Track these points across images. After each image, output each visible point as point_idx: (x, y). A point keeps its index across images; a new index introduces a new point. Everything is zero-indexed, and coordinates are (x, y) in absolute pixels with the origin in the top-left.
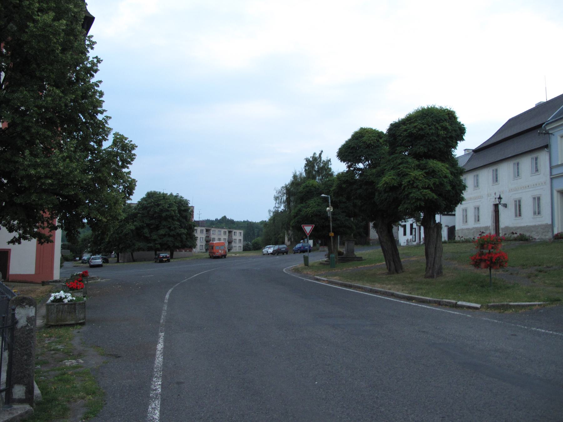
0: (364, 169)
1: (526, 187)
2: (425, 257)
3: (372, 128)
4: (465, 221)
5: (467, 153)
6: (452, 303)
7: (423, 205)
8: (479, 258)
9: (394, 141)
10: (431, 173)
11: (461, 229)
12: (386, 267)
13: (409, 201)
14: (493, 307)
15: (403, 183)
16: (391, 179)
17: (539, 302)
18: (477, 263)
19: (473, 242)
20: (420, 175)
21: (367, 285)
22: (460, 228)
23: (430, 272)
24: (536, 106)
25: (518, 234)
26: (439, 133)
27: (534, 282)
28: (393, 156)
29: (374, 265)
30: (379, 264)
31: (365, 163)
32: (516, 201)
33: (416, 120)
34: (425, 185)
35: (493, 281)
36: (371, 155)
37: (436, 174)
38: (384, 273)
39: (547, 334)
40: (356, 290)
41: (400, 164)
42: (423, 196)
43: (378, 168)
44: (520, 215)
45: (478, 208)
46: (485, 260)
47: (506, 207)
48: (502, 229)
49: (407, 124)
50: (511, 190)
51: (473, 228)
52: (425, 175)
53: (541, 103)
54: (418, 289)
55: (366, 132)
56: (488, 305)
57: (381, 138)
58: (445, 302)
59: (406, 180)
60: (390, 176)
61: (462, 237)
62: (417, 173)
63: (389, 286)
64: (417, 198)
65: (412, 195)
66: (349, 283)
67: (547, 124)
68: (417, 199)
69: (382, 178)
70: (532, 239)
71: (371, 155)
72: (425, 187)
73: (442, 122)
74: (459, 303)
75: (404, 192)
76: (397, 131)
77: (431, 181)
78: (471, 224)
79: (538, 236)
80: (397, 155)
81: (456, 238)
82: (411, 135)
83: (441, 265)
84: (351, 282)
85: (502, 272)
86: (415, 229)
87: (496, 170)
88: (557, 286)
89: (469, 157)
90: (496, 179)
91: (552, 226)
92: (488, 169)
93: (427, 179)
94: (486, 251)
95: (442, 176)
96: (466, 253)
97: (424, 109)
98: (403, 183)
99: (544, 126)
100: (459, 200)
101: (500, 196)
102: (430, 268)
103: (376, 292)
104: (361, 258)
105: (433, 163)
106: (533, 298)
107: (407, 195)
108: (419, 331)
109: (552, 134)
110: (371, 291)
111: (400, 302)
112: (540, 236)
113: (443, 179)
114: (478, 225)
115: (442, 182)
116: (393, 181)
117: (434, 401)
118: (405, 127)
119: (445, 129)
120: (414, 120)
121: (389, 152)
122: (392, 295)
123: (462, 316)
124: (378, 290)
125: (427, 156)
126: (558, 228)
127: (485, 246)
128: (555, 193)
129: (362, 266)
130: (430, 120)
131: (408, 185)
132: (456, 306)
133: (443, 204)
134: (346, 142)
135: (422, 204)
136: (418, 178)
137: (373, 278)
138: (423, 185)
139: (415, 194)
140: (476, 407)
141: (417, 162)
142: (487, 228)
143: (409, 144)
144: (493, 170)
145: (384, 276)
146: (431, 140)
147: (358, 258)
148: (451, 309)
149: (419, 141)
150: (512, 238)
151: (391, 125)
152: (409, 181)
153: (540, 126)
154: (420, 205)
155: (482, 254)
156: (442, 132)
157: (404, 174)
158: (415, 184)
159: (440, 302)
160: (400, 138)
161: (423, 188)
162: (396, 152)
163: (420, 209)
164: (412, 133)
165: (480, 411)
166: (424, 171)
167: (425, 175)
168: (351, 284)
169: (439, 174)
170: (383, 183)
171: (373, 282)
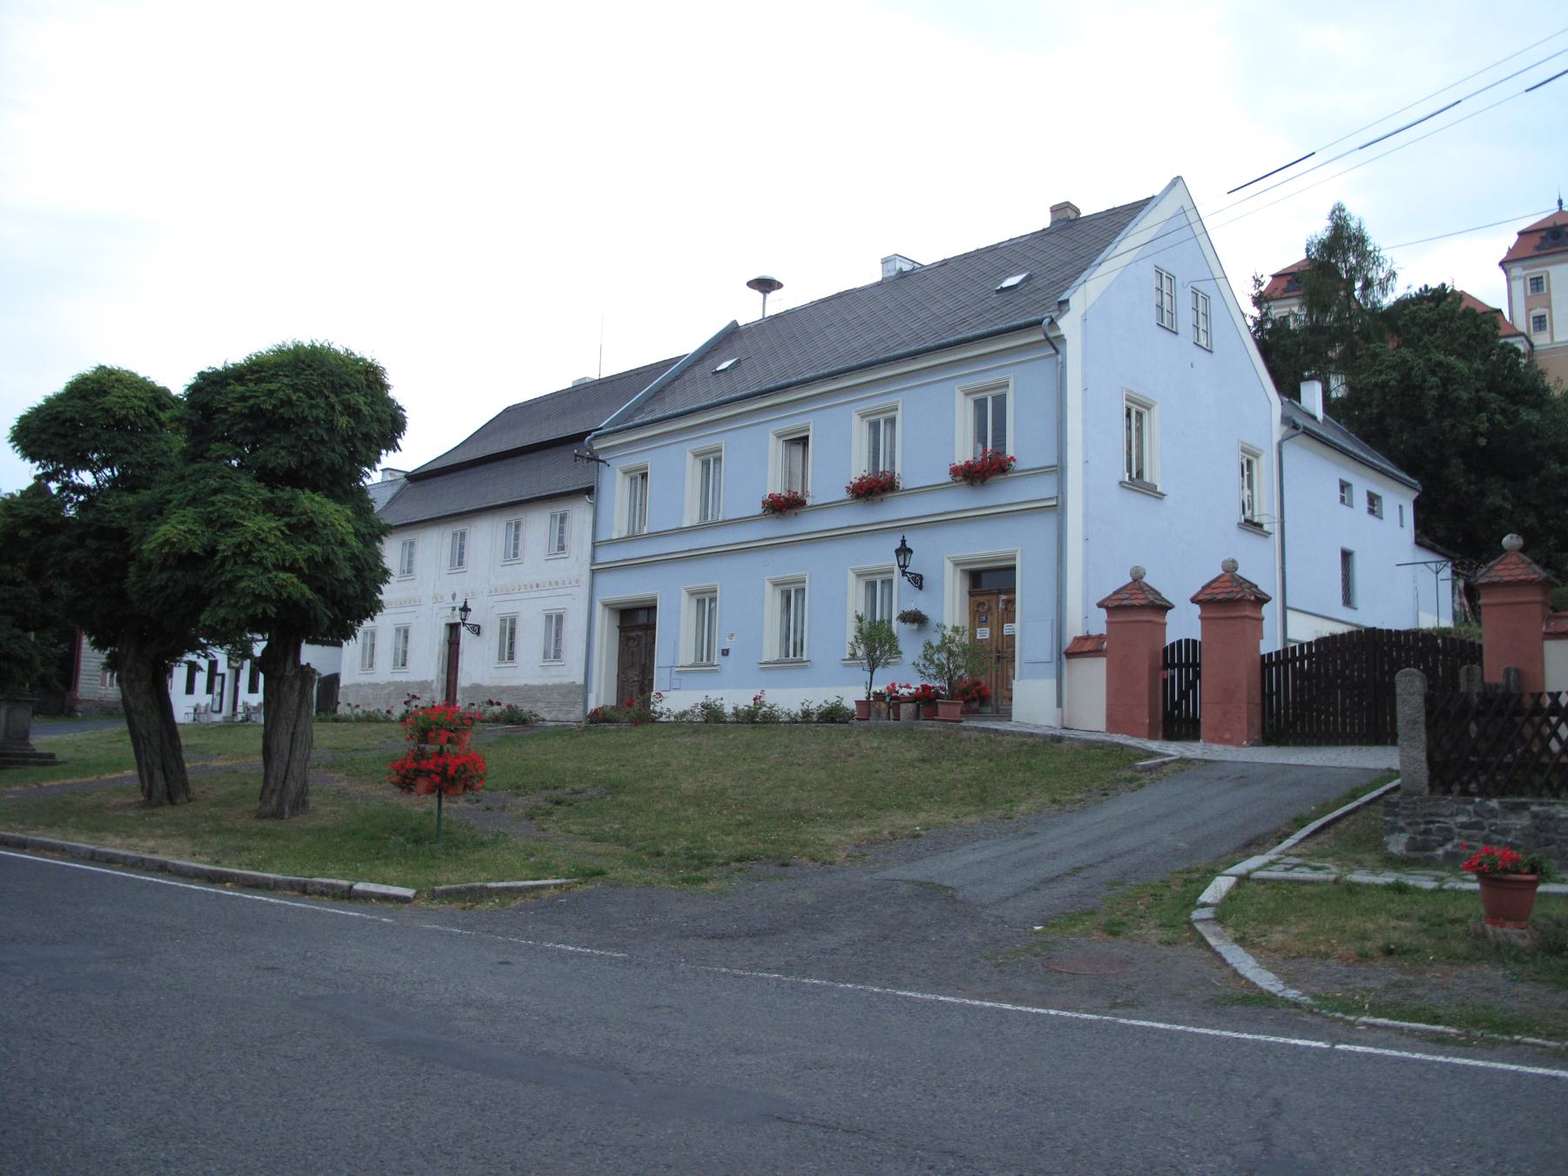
0: (95, 489)
1: (531, 587)
2: (259, 760)
3: (134, 371)
4: (369, 662)
5: (390, 478)
6: (341, 887)
7: (273, 616)
8: (415, 764)
9: (203, 423)
10: (304, 529)
11: (352, 685)
12: (137, 782)
13: (233, 601)
14: (448, 894)
15: (222, 547)
16: (185, 532)
17: (556, 878)
18: (406, 780)
19: (387, 720)
20: (271, 529)
21: (79, 841)
22: (352, 682)
23: (274, 801)
24: (574, 387)
25: (504, 707)
26: (335, 422)
27: (543, 830)
28: (196, 466)
29: (95, 777)
30: (114, 776)
31: (100, 470)
32: (503, 620)
33: (276, 375)
34: (284, 560)
35: (443, 828)
36: (125, 451)
37: (317, 532)
38: (129, 805)
39: (579, 955)
40: (43, 857)
41: (216, 492)
42: (276, 590)
43: (145, 495)
44: (511, 658)
45: (406, 632)
46: (429, 773)
47: (478, 634)
48: (464, 689)
49: (250, 380)
50: (496, 590)
51: (389, 683)
52: (287, 532)
53: (587, 381)
54: (240, 850)
55: (117, 380)
56: (434, 891)
57: (163, 407)
58: (321, 883)
59: (230, 541)
60: (183, 523)
61: (358, 706)
62: (264, 524)
63: (151, 843)
64: (260, 593)
65: (243, 584)
66: (17, 835)
67: (596, 437)
68: (259, 598)
69: (158, 525)
70: (536, 721)
71: (125, 451)
72: (284, 564)
73: (348, 393)
74: (359, 886)
75: (223, 573)
76: (217, 397)
77: (300, 549)
78: (384, 672)
79: (550, 712)
80: (208, 464)
81: (339, 708)
82: (255, 413)
83: (305, 784)
84: (21, 831)
85: (466, 804)
86: (223, 675)
87: (463, 535)
88: (596, 840)
89: (395, 489)
90: (459, 559)
91: (586, 688)
92: (442, 529)
93: (292, 542)
94: (431, 748)
95: (333, 541)
96: (368, 750)
97: (303, 346)
98: (222, 547)
99: (590, 441)
100: (368, 606)
101: (466, 603)
102: (273, 791)
103: (110, 860)
104: (52, 756)
105: (313, 500)
106: (543, 869)
107: (230, 584)
108: (259, 967)
109: (604, 461)
110: (93, 857)
111: (187, 889)
112: (554, 713)
113: (335, 548)
114: (401, 677)
115: (332, 557)
116: (191, 538)
117: (330, 1148)
118: (241, 389)
119: (353, 412)
120: (271, 372)
121: (184, 452)
122: (162, 868)
123: (370, 920)
124: (115, 855)
125: (294, 479)
126: (598, 696)
127: (432, 735)
128: (599, 608)
129: (56, 783)
130: (315, 378)
131: (234, 554)
132: (349, 895)
133: (324, 613)
134: (48, 400)
135: (269, 612)
136: (266, 537)
137: (96, 818)
138: (277, 560)
139: (253, 582)
140: (439, 1146)
141: (265, 493)
142: (425, 686)
143: (249, 438)
144: (455, 535)
145: (132, 814)
147: (41, 755)
148: (337, 903)
149: (277, 435)
150: (487, 715)
151: (202, 375)
152: (239, 545)
153: (579, 438)
154: (264, 612)
155: (422, 753)
156: (343, 422)
157: (224, 521)
158: (255, 555)
159: (305, 884)
160: (224, 417)
161: (277, 567)
162: (208, 455)
163: (258, 625)
164: (261, 410)
165: (448, 1154)
166: (286, 519)
167: (287, 532)
168: (24, 836)
169: (327, 534)
170: (160, 540)
171: (98, 830)
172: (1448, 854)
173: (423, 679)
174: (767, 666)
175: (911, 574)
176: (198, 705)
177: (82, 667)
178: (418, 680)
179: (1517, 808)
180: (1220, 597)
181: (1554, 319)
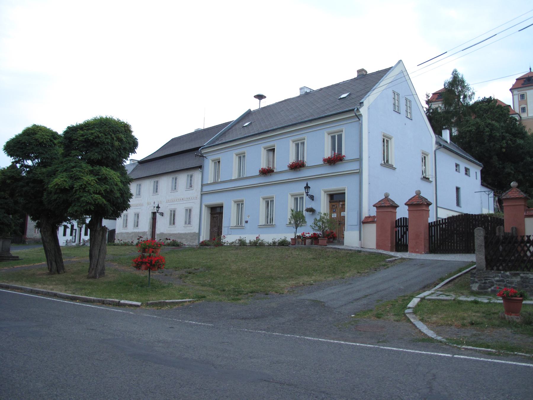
0: (32, 166)
1: (181, 200)
2: (88, 258)
3: (46, 126)
4: (126, 225)
5: (132, 163)
6: (116, 302)
7: (93, 209)
8: (141, 260)
9: (69, 144)
10: (103, 180)
11: (120, 233)
12: (47, 266)
13: (79, 204)
14: (152, 304)
15: (75, 186)
16: (63, 181)
17: (189, 299)
18: (138, 265)
19: (132, 245)
20: (92, 180)
21: (27, 286)
22: (120, 232)
23: (93, 272)
24: (195, 132)
25: (171, 240)
27: (185, 282)
28: (67, 159)
29: (32, 264)
30: (39, 264)
32: (171, 211)
33: (94, 128)
34: (96, 191)
35: (151, 282)
36: (42, 153)
37: (108, 181)
38: (44, 274)
39: (197, 325)
40: (15, 291)
41: (73, 167)
42: (94, 201)
43: (49, 169)
44: (174, 224)
45: (138, 215)
46: (146, 263)
47: (163, 216)
48: (158, 235)
49: (85, 129)
50: (169, 201)
51: (132, 232)
52: (97, 181)
53: (200, 129)
54: (81, 289)
55: (40, 129)
56: (147, 303)
57: (55, 138)
58: (109, 300)
59: (78, 184)
60: (62, 178)
61: (122, 240)
62: (90, 178)
63: (51, 287)
64: (88, 202)
65: (83, 199)
66: (6, 284)
67: (203, 149)
68: (88, 203)
69: (54, 179)
70: (182, 245)
71: (42, 153)
72: (96, 192)
73: (118, 134)
74: (122, 301)
75: (76, 195)
76: (74, 135)
77: (102, 187)
78: (131, 228)
79: (187, 242)
80: (71, 158)
81: (115, 241)
82: (87, 141)
83: (104, 267)
84: (7, 283)
85: (158, 274)
86: (76, 230)
87: (157, 182)
88: (202, 286)
89: (134, 166)
90: (156, 190)
91: (199, 234)
92: (150, 180)
93: (99, 185)
94: (146, 254)
95: (113, 184)
96: (125, 255)
97: (103, 118)
98: (75, 186)
99: (200, 150)
100: (125, 206)
101: (158, 205)
102: (93, 269)
103: (37, 293)
104: (18, 257)
105: (106, 170)
106: (185, 296)
107: (78, 199)
108: (88, 329)
109: (205, 157)
110: (32, 292)
111: (64, 302)
112: (188, 242)
113: (114, 186)
114: (136, 230)
115: (113, 190)
116: (65, 183)
117: (112, 390)
118: (82, 132)
119: (120, 140)
120: (92, 127)
121: (62, 154)
122: (55, 295)
123: (126, 313)
124: (39, 291)
125: (100, 163)
126: (203, 237)
127: (147, 250)
128: (203, 207)
129: (19, 266)
130: (107, 129)
131: (80, 188)
132: (119, 305)
133: (110, 208)
134: (16, 136)
136: (91, 183)
137: (32, 278)
138: (94, 190)
139: (86, 198)
140: (149, 390)
141: (90, 168)
142: (144, 233)
144: (155, 182)
145: (45, 277)
146: (106, 148)
147: (14, 257)
148: (115, 307)
149: (94, 148)
150: (166, 243)
151: (69, 128)
152: (81, 185)
153: (197, 149)
154: (90, 208)
155: (143, 256)
156: (117, 143)
157: (76, 177)
158: (87, 189)
159: (104, 301)
160: (76, 142)
161: (94, 193)
162: (71, 155)
163: (88, 213)
164: (89, 139)
165: (152, 392)
166: (97, 177)
167: (97, 181)
168: (8, 284)
169: (111, 182)
170: (54, 184)
171: (33, 282)
172: (492, 291)
173: (144, 231)
174: (261, 227)
175: (310, 195)
176: (67, 240)
177: (28, 227)
178: (142, 231)
179: (516, 275)
180: (415, 203)
181: (528, 108)
